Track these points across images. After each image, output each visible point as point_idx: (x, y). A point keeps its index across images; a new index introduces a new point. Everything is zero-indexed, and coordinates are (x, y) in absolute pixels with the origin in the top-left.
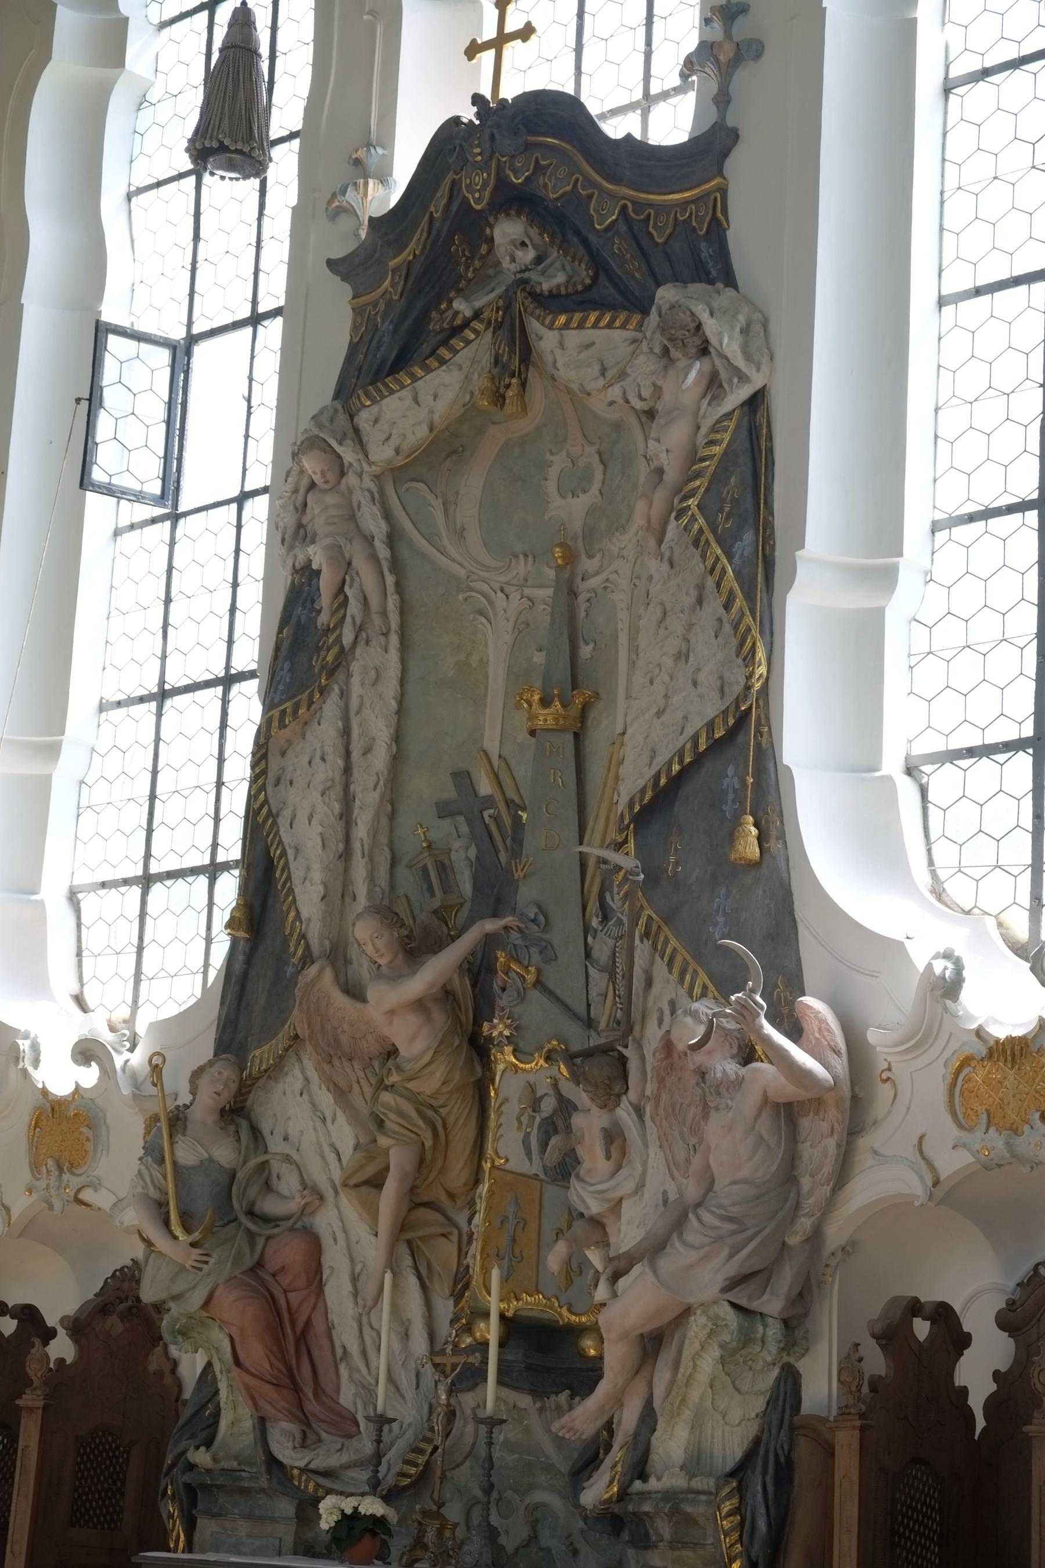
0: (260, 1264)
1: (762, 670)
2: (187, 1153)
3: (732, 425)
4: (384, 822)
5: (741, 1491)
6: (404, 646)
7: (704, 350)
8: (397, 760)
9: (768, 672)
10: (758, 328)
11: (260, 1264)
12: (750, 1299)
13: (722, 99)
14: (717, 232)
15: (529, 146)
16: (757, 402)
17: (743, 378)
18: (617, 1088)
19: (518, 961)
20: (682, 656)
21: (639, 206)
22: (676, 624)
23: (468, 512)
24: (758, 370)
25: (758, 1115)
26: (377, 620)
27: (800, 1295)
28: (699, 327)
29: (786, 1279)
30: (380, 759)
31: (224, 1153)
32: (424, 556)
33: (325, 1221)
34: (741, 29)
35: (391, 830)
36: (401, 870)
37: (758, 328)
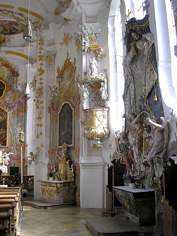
0: (128, 154)
1: (157, 77)
2: (120, 143)
3: (151, 48)
4: (134, 103)
5: (161, 180)
6: (134, 83)
7: (147, 41)
8: (135, 95)
9: (157, 77)
10: (152, 36)
11: (128, 154)
12: (159, 156)
13: (147, 12)
14: (148, 27)
15: (132, 25)
16: (153, 45)
17: (151, 43)
18: (150, 131)
19: (145, 117)
20: (150, 78)
21: (141, 27)
22: (149, 74)
23: (139, 67)
24: (152, 41)
25: (158, 133)
26: (131, 81)
27: (165, 154)
28: (145, 38)
29: (163, 153)
30: (133, 96)
31: (124, 142)
32: (135, 73)
33: (133, 149)
34: (148, 3)
35: (135, 104)
36: (137, 108)
37: (152, 36)
